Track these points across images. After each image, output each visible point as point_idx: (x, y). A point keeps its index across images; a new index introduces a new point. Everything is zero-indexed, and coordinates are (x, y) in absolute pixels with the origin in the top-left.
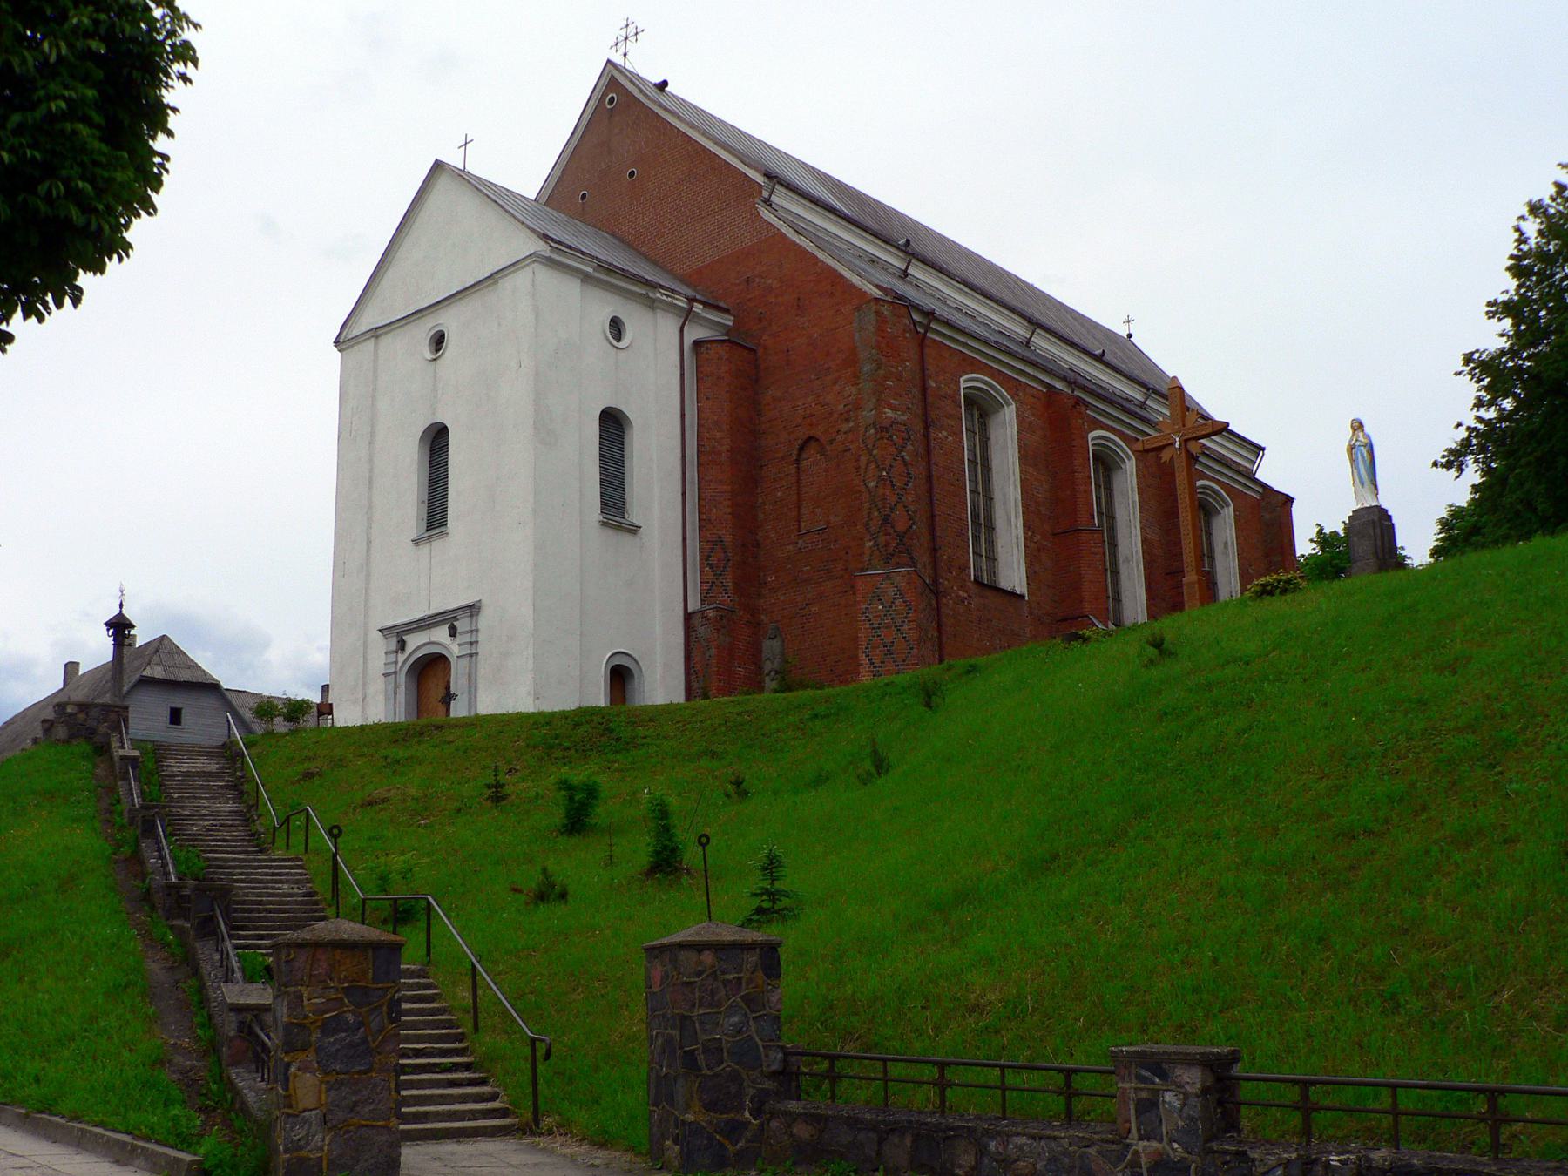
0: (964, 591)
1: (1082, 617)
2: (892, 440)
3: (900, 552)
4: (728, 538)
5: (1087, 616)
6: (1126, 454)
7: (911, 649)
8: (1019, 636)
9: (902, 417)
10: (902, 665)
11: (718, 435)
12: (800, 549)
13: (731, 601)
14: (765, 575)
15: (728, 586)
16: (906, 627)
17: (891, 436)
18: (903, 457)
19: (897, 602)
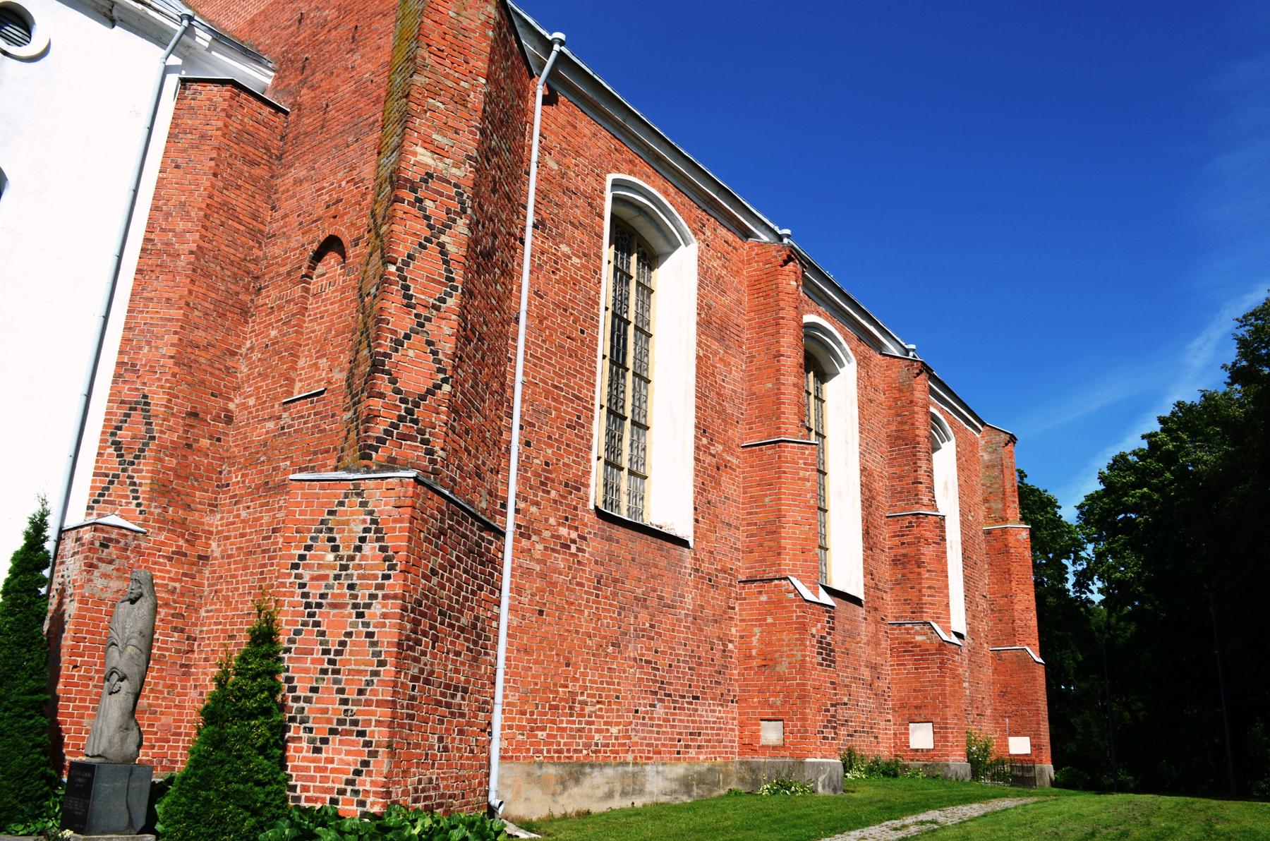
0: (570, 527)
1: (780, 579)
2: (422, 209)
3: (403, 437)
4: (158, 400)
5: (786, 579)
6: (846, 355)
7: (382, 663)
8: (674, 607)
9: (454, 171)
10: (356, 703)
11: (181, 225)
12: (283, 428)
13: (141, 512)
14: (230, 472)
15: (141, 485)
16: (377, 608)
17: (420, 201)
18: (442, 245)
19: (366, 548)
